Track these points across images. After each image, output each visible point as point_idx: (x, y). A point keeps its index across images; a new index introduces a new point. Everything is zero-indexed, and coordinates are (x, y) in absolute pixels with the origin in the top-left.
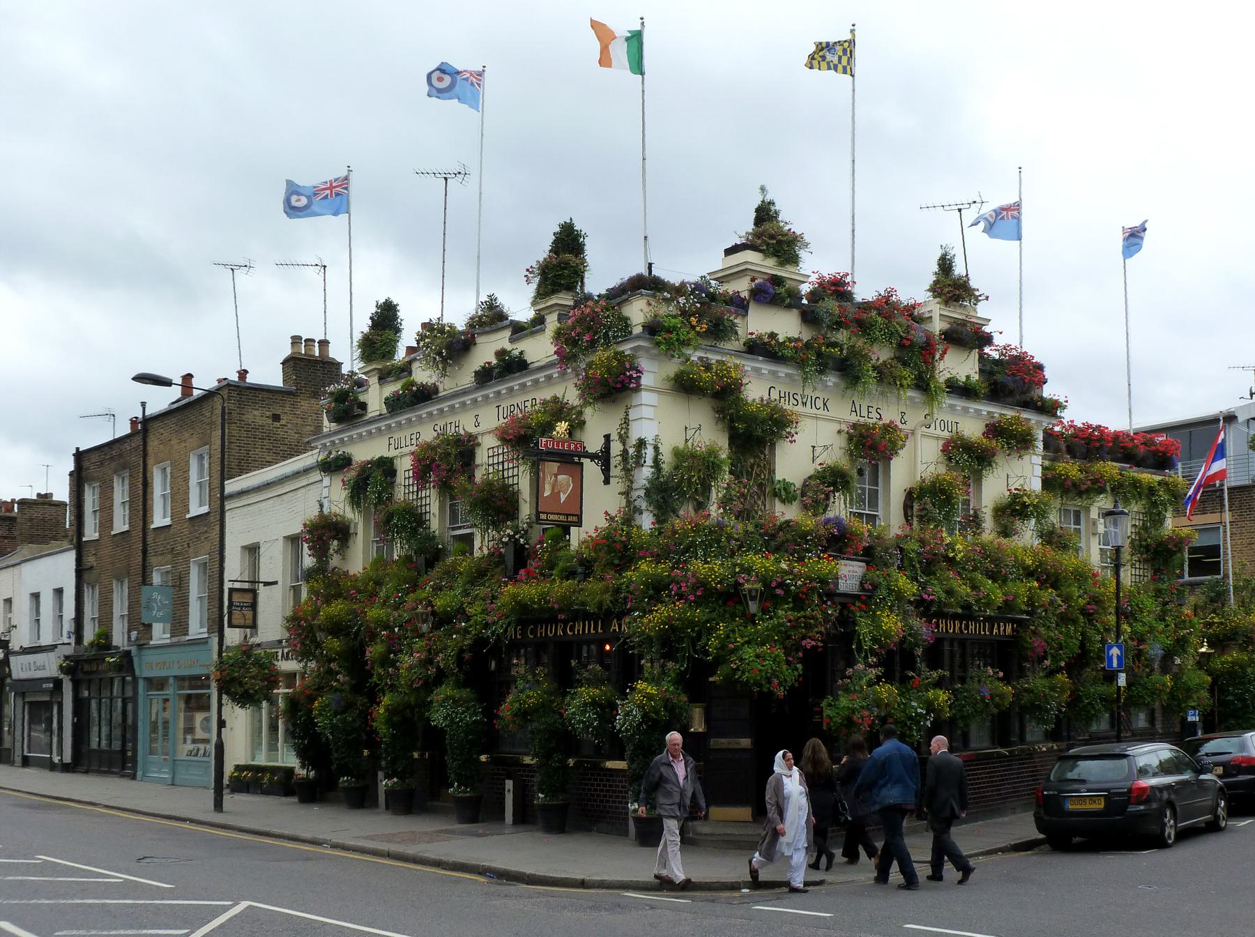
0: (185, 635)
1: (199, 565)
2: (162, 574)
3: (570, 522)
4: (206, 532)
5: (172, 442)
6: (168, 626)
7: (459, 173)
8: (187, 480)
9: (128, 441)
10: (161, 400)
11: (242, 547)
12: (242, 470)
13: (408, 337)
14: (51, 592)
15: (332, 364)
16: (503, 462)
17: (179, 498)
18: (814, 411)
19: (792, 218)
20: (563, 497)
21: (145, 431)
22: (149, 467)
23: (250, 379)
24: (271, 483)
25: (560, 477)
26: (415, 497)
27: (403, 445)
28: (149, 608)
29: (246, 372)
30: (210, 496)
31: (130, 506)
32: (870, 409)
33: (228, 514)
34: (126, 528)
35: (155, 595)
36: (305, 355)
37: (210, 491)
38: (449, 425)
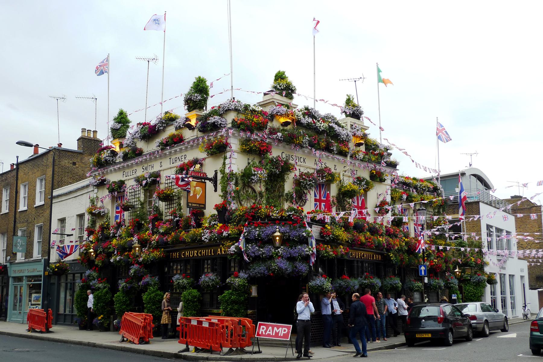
0: (31, 258)
1: (39, 228)
2: (22, 231)
3: (201, 207)
4: (42, 213)
5: (29, 174)
6: (24, 254)
7: (154, 59)
8: (35, 190)
9: (10, 173)
10: (26, 154)
11: (58, 219)
12: (59, 186)
13: (133, 129)
14: (57, 221)
15: (98, 141)
16: (172, 182)
17: (31, 198)
18: (301, 164)
19: (292, 78)
20: (198, 197)
21: (18, 168)
22: (19, 184)
23: (63, 147)
24: (72, 191)
25: (197, 188)
26: (134, 197)
27: (129, 175)
28: (16, 246)
29: (61, 144)
30: (45, 197)
31: (9, 201)
32: (322, 163)
33: (53, 205)
34: (7, 211)
35: (19, 240)
36: (87, 137)
37: (45, 195)
38: (149, 166)
